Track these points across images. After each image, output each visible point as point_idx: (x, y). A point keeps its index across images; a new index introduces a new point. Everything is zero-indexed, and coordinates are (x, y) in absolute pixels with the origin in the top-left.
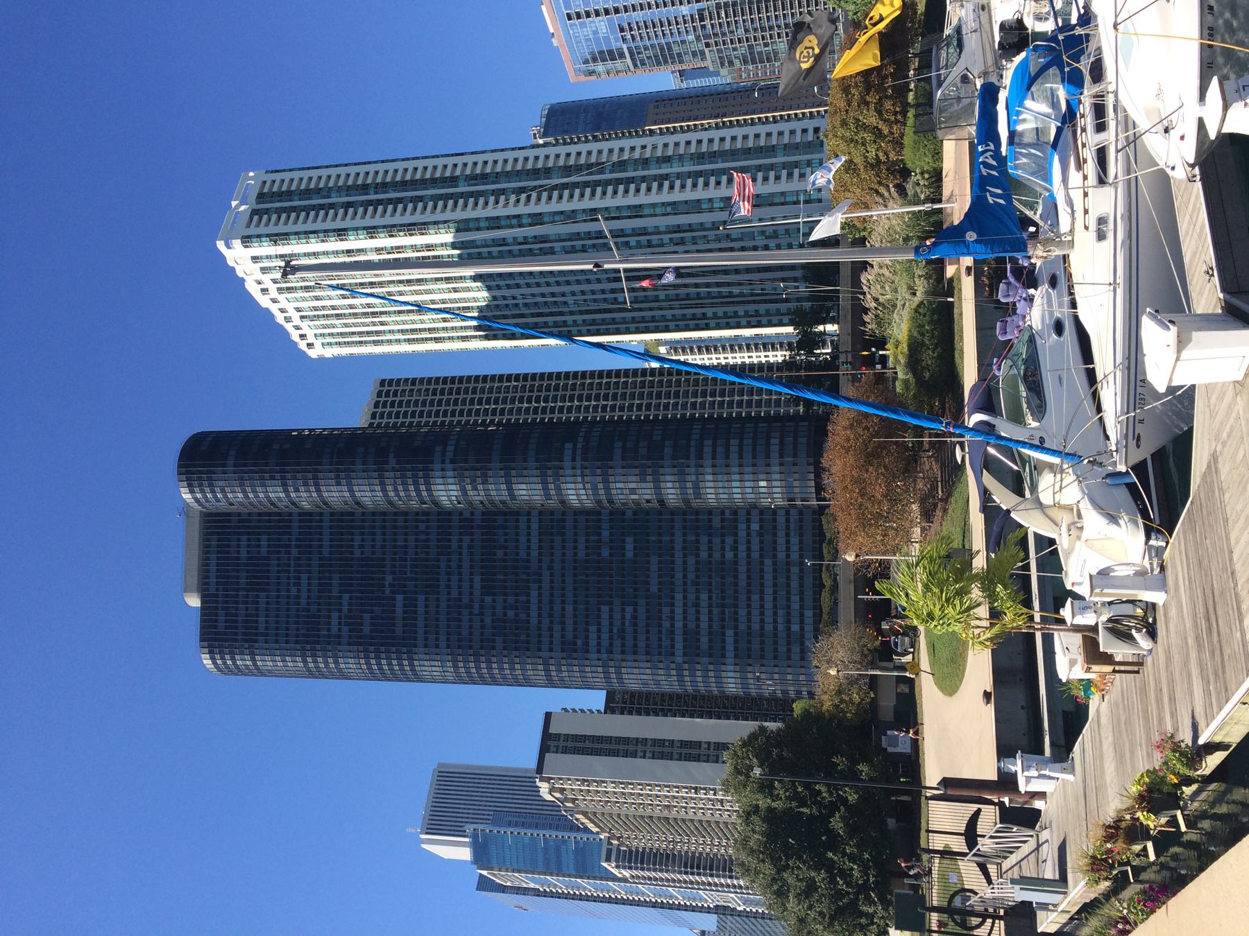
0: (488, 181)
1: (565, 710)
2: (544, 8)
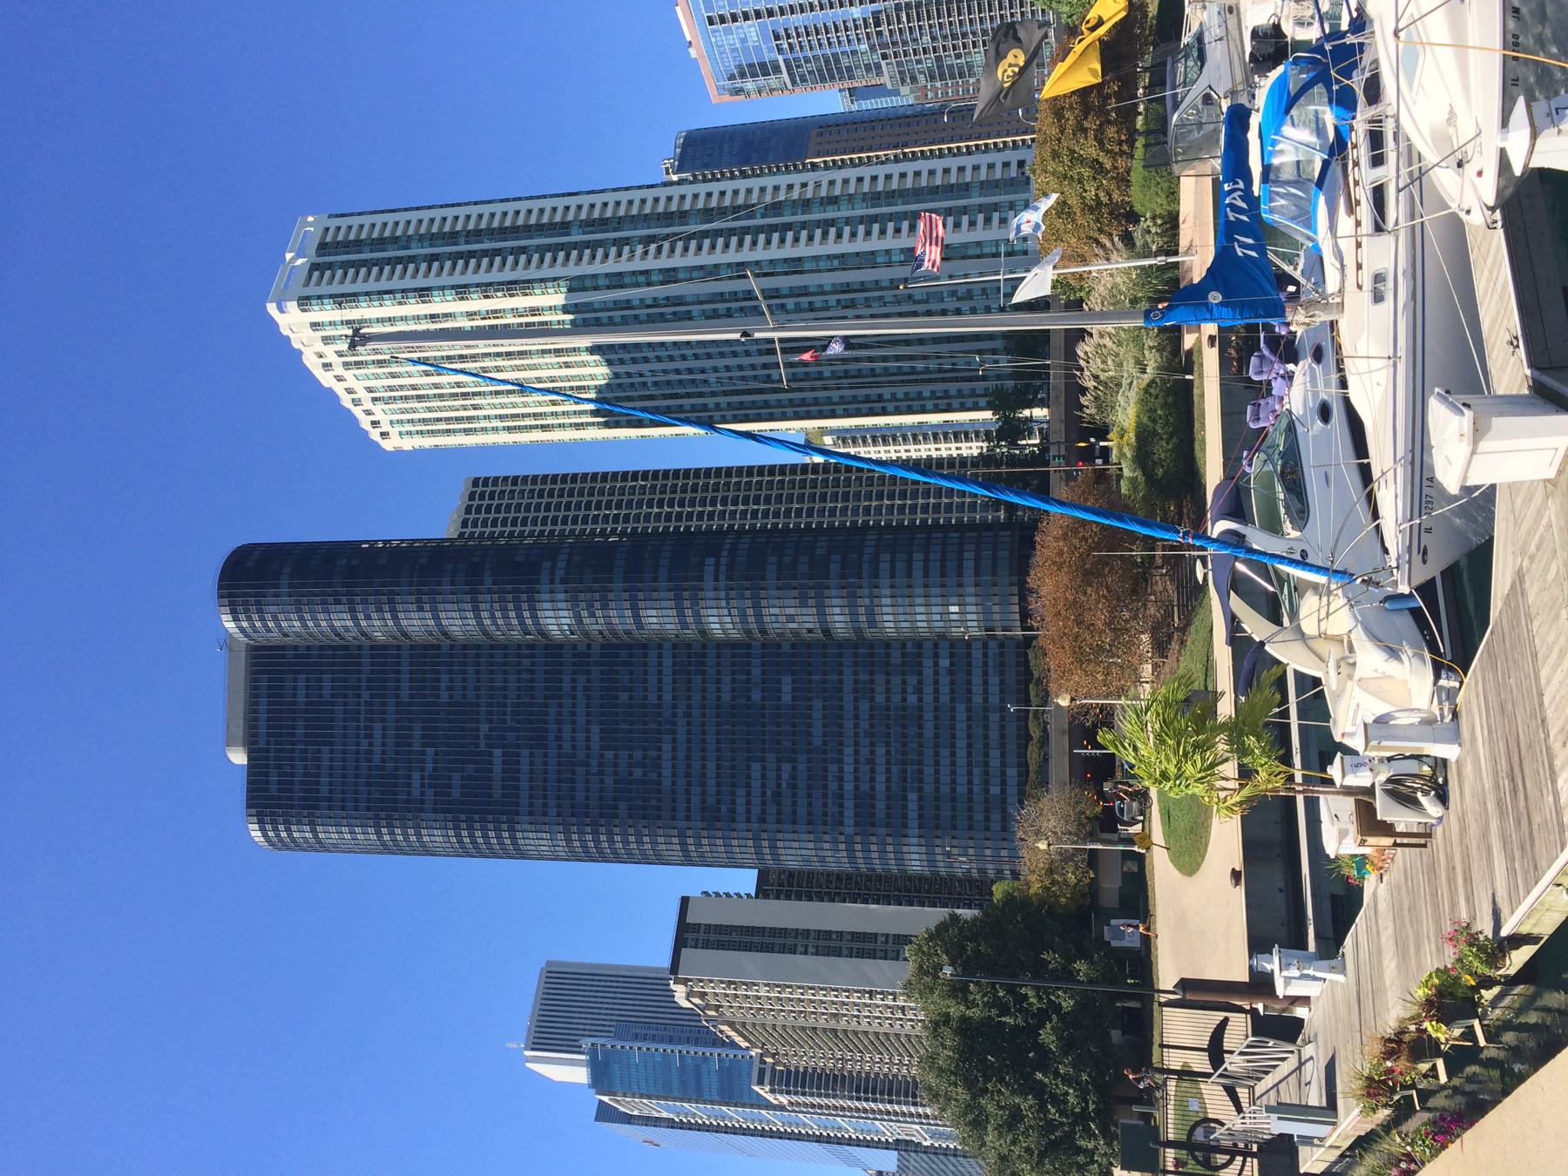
2: (678, 9)
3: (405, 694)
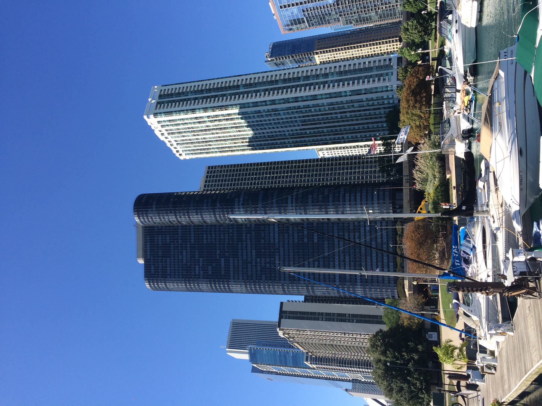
0: (251, 87)
1: (289, 301)
2: (270, 3)
3: (192, 241)
